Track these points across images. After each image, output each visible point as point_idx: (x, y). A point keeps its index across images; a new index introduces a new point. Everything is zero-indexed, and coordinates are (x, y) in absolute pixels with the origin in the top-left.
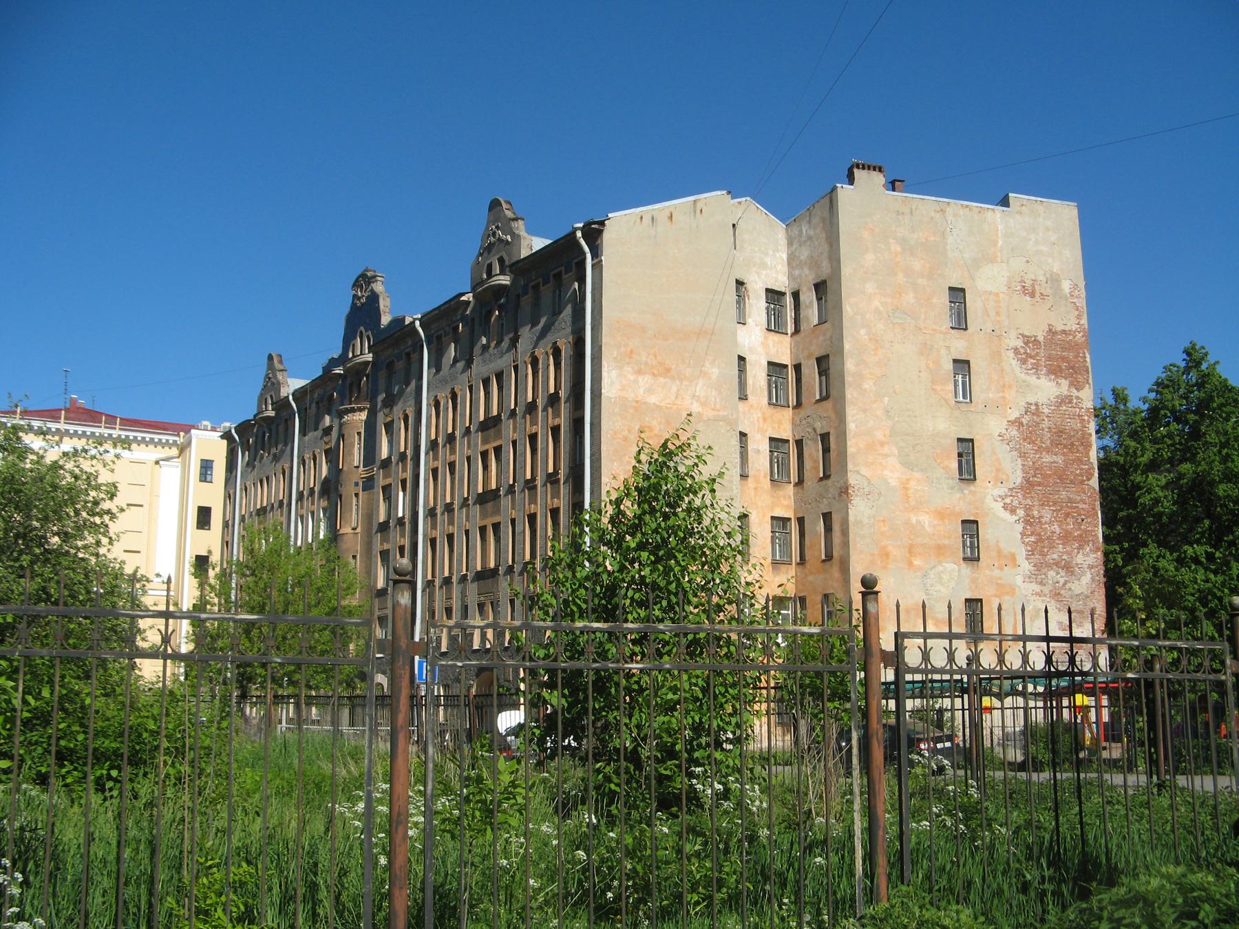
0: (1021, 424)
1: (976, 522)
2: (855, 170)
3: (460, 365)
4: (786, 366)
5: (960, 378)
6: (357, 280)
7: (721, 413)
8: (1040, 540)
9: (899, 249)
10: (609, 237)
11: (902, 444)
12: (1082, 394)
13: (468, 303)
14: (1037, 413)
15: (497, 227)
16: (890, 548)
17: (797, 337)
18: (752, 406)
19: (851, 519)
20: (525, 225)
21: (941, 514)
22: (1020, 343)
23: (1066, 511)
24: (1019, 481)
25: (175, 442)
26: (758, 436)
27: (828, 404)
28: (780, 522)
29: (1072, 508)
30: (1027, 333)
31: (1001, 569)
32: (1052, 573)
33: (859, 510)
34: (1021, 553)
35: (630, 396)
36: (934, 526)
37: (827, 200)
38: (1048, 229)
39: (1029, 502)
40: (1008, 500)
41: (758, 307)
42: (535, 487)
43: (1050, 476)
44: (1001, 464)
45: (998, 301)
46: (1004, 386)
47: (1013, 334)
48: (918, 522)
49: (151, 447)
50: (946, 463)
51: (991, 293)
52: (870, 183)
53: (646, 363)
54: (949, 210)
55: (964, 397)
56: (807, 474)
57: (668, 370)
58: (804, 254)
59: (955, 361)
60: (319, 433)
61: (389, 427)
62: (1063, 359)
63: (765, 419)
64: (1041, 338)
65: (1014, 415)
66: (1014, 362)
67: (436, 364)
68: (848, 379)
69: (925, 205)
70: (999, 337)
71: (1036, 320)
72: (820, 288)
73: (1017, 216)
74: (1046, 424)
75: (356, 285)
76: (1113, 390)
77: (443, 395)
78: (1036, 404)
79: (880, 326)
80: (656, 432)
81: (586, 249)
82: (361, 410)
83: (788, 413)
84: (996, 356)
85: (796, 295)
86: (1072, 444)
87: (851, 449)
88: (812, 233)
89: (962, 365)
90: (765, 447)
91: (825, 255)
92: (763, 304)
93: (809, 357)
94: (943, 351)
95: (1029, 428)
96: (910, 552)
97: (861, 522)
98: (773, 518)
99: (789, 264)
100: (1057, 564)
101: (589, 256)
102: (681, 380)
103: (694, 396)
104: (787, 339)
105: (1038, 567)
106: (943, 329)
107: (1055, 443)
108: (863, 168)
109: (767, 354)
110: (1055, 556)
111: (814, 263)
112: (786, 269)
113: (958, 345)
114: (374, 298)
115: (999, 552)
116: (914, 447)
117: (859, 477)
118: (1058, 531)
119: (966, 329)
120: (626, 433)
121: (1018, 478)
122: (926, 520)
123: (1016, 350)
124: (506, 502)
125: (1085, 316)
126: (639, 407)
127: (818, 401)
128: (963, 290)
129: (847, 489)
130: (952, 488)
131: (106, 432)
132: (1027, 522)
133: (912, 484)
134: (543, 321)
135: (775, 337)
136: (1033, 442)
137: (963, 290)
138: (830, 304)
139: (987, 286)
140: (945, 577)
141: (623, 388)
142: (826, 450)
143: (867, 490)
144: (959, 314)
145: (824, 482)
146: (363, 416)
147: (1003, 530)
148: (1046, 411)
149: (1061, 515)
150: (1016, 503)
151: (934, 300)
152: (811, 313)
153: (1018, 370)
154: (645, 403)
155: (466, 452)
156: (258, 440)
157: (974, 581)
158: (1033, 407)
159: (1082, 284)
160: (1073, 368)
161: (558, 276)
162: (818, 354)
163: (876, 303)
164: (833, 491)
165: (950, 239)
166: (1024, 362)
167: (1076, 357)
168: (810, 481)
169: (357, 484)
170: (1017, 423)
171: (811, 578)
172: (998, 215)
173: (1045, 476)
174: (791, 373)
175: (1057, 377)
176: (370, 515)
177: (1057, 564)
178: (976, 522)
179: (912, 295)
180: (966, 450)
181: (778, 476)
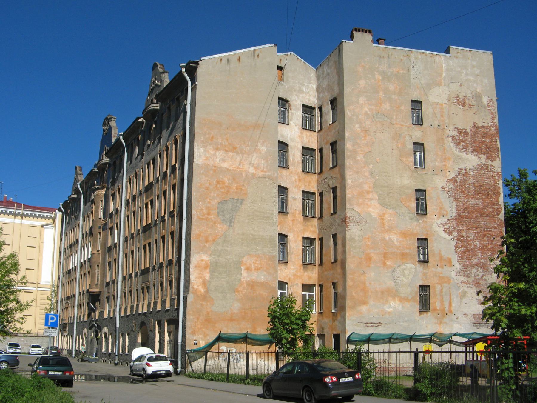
0: (456, 181)
1: (427, 239)
2: (354, 32)
3: (139, 157)
4: (314, 150)
5: (418, 154)
6: (104, 122)
7: (267, 174)
8: (467, 250)
9: (381, 78)
10: (201, 71)
11: (381, 192)
12: (494, 164)
13: (143, 123)
14: (466, 174)
15: (156, 79)
16: (372, 255)
17: (321, 133)
18: (291, 172)
19: (348, 237)
20: (169, 75)
21: (404, 234)
22: (455, 133)
23: (483, 233)
24: (454, 215)
25: (51, 216)
26: (295, 190)
27: (336, 170)
28: (308, 241)
29: (487, 231)
30: (460, 127)
31: (442, 267)
32: (474, 270)
33: (353, 232)
34: (455, 258)
35: (212, 163)
36: (400, 242)
37: (337, 50)
38: (473, 67)
39: (460, 227)
40: (447, 227)
41: (296, 116)
42: (165, 220)
43: (474, 212)
44: (443, 206)
45: (442, 109)
46: (445, 159)
47: (451, 128)
48: (390, 239)
49: (40, 219)
50: (408, 204)
51: (438, 104)
52: (363, 39)
53: (221, 144)
54: (412, 56)
55: (421, 165)
56: (325, 212)
57: (235, 148)
58: (325, 83)
59: (415, 144)
60: (90, 203)
61: (113, 195)
62: (483, 143)
63: (300, 180)
64: (469, 131)
65: (452, 175)
66: (452, 145)
67: (130, 159)
68: (347, 153)
69: (398, 53)
70: (443, 129)
71: (465, 120)
72: (333, 102)
73: (455, 59)
74: (471, 181)
75: (104, 124)
76: (519, 171)
77: (132, 175)
78: (466, 170)
79: (368, 123)
80: (227, 184)
81: (188, 78)
82: (102, 188)
83: (315, 177)
84: (440, 141)
85: (321, 109)
86: (488, 194)
87: (348, 195)
88: (329, 71)
89: (419, 146)
90: (300, 196)
91: (336, 82)
92: (300, 113)
93: (326, 143)
94: (407, 138)
95: (460, 184)
96: (384, 257)
97: (353, 239)
98: (304, 238)
99: (317, 91)
100: (477, 265)
101: (190, 83)
102: (243, 154)
103: (250, 163)
104: (316, 134)
105: (465, 266)
106: (407, 124)
107: (477, 193)
108: (359, 31)
109: (302, 142)
110: (476, 260)
111: (330, 88)
112: (315, 94)
113: (417, 134)
114: (110, 129)
115: (441, 257)
116: (388, 194)
117: (353, 212)
118: (478, 245)
119: (422, 125)
120: (208, 185)
121: (454, 213)
122: (395, 238)
123: (453, 138)
124: (153, 230)
125: (497, 118)
126: (216, 170)
127: (331, 168)
128: (420, 102)
129: (346, 219)
130: (412, 219)
131: (17, 211)
132: (458, 239)
133: (387, 216)
134: (171, 125)
135: (308, 133)
136: (463, 192)
137: (420, 102)
138: (338, 111)
139: (436, 99)
140: (407, 272)
141: (207, 159)
142: (335, 197)
143: (358, 220)
144: (418, 117)
145: (333, 216)
146: (104, 191)
147: (443, 244)
148: (472, 173)
149: (480, 236)
150: (452, 228)
151: (402, 108)
152: (329, 117)
153: (454, 149)
154: (221, 167)
155: (140, 205)
156: (70, 209)
157: (425, 274)
158: (464, 171)
159: (495, 99)
160: (489, 148)
161: (178, 99)
162: (331, 141)
163: (366, 109)
164: (338, 221)
165: (413, 72)
166: (458, 144)
167: (491, 142)
168: (326, 217)
169: (100, 227)
170: (453, 180)
171: (326, 273)
172: (443, 58)
173: (470, 212)
174: (317, 153)
175: (479, 153)
176: (105, 243)
177: (477, 265)
178: (427, 239)
179: (388, 105)
180: (421, 198)
181: (308, 212)
